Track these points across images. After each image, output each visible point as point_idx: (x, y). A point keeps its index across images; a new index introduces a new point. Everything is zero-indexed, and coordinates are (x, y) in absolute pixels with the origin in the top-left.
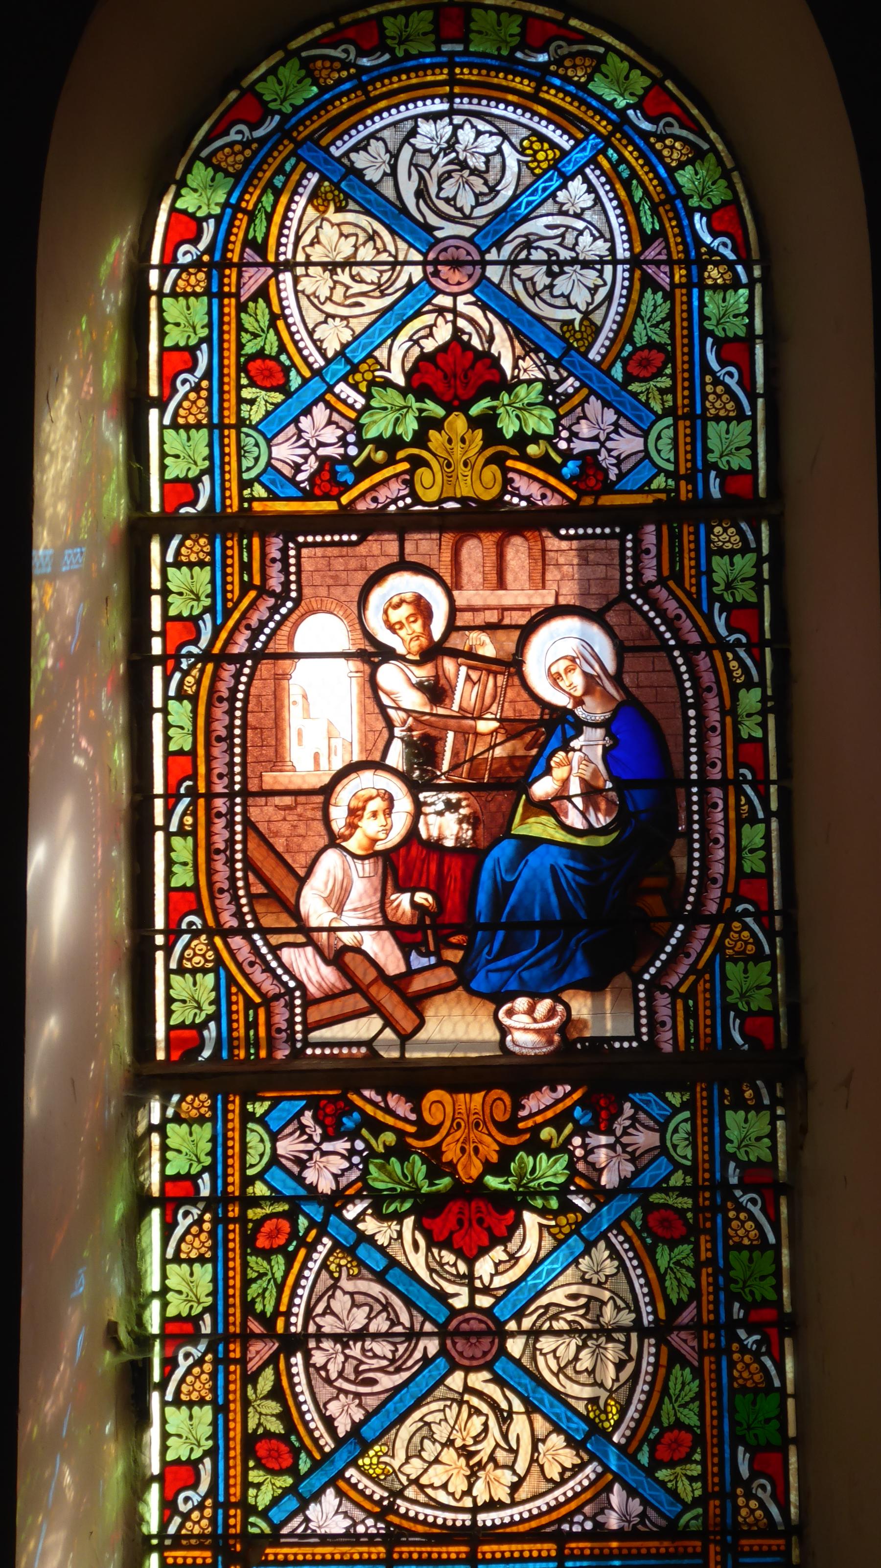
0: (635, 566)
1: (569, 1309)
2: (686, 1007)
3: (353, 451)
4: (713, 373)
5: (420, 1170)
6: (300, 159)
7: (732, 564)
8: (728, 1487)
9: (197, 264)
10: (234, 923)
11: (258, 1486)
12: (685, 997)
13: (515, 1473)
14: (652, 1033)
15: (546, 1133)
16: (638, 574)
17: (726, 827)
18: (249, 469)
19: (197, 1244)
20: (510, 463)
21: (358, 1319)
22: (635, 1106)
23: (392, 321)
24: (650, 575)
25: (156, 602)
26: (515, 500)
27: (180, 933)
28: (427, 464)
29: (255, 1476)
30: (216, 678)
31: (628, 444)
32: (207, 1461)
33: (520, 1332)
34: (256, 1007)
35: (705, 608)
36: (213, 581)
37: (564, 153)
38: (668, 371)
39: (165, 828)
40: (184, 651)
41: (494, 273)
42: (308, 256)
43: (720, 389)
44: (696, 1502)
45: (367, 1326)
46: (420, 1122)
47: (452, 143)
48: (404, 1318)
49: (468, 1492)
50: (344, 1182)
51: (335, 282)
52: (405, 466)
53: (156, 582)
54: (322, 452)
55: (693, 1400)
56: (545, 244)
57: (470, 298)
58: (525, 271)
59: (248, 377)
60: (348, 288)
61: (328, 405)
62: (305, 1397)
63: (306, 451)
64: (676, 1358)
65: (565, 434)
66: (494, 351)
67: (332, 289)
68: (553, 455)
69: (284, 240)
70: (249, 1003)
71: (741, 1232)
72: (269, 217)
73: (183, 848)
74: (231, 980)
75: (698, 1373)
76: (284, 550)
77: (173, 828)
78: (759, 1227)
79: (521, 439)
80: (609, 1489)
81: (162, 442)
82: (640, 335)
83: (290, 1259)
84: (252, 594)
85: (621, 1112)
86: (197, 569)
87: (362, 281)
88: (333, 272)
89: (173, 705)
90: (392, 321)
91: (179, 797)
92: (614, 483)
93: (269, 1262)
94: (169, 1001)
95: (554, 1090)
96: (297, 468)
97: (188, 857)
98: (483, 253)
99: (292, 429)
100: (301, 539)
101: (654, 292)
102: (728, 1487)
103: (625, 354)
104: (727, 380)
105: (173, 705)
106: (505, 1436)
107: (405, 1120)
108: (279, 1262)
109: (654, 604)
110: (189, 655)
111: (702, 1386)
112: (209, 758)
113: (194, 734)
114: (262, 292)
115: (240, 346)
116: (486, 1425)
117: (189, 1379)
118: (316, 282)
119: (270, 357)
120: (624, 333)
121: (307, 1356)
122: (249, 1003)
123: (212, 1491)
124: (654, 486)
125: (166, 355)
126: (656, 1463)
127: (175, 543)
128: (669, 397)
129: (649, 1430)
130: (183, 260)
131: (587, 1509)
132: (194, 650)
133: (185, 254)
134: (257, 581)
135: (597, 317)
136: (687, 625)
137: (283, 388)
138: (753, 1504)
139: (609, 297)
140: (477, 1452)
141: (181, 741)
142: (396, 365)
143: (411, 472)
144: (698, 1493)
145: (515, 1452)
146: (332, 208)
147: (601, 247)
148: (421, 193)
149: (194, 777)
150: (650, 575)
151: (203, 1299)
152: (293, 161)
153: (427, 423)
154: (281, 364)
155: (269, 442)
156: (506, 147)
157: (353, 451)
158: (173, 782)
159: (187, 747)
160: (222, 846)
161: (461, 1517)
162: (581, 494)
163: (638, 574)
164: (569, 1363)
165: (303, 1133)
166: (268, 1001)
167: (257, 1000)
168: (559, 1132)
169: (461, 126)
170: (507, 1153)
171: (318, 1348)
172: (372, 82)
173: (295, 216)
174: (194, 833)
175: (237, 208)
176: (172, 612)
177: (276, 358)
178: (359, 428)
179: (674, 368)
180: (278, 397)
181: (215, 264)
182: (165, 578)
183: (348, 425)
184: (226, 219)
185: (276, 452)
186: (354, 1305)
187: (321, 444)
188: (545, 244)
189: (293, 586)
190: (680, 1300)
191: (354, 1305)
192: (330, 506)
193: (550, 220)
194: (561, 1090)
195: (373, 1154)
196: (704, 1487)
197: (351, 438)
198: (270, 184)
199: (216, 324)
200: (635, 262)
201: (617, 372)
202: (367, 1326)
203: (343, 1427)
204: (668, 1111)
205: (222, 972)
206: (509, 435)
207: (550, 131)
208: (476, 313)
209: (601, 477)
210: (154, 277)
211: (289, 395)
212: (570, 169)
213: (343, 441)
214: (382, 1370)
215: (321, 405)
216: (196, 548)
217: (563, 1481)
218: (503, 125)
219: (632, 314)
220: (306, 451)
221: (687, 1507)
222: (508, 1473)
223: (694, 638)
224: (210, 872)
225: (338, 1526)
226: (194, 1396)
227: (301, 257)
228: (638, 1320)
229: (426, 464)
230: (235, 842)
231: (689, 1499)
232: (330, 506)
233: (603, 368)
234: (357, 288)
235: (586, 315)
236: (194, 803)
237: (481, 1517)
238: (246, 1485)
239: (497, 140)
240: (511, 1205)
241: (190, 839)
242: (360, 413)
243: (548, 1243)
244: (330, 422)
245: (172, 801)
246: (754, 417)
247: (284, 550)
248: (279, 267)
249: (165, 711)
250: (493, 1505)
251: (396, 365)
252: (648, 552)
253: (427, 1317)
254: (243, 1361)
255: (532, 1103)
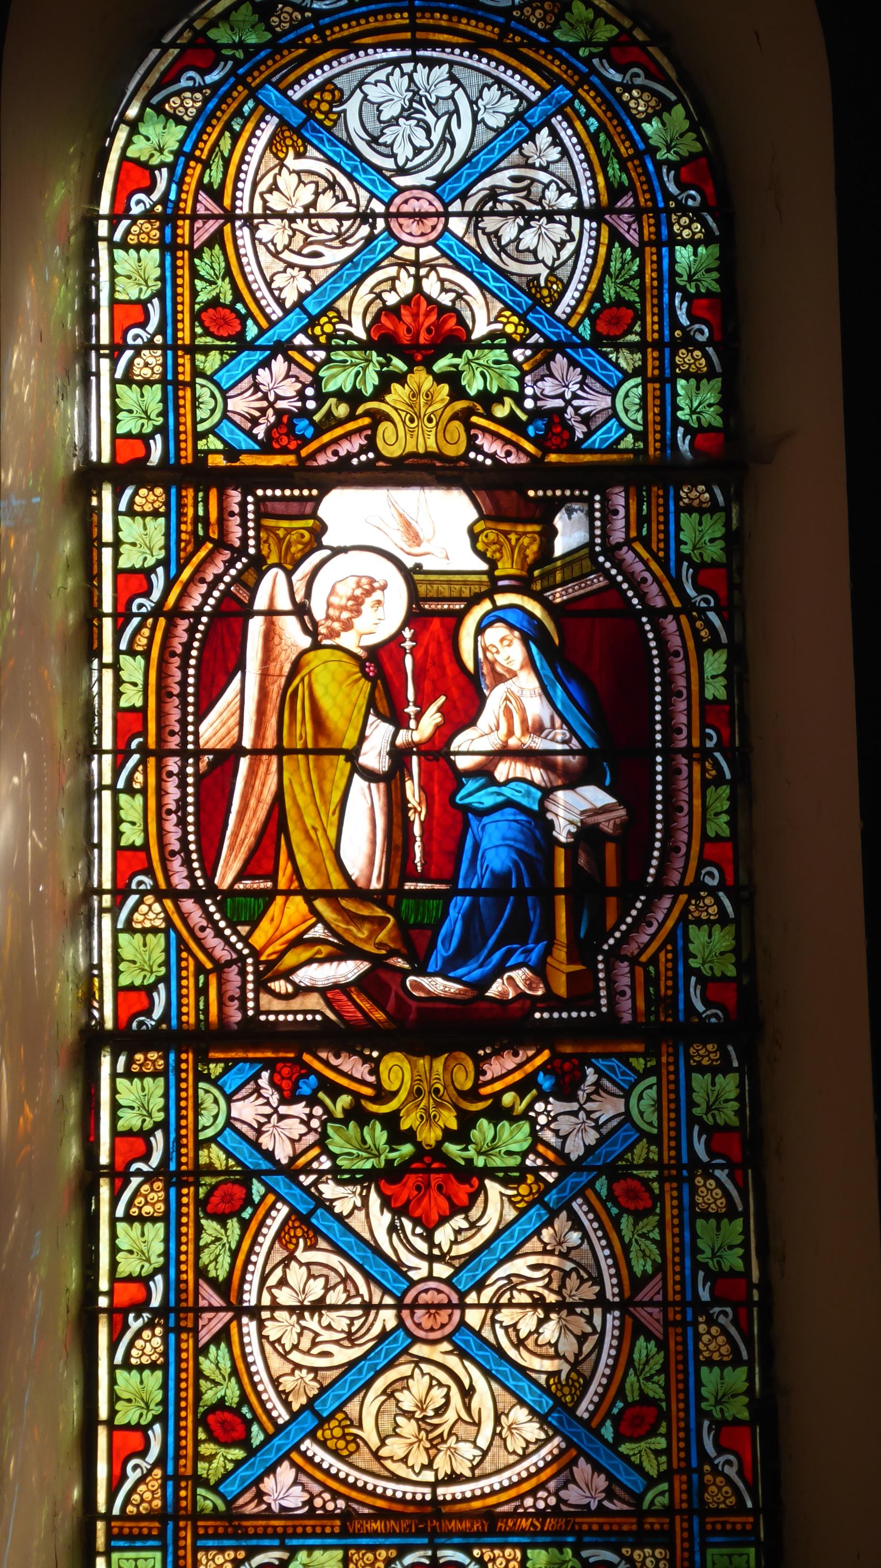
0: (603, 528)
1: (322, 243)
2: (647, 973)
3: (311, 405)
4: (710, 1461)
5: (379, 1135)
6: (258, 102)
7: (713, 1084)
8: (694, 1464)
9: (148, 215)
10: (185, 885)
11: (210, 1459)
12: (645, 966)
13: (476, 1447)
14: (612, 1003)
15: (508, 1099)
16: (605, 536)
17: (691, 795)
18: (650, 1087)
19: (148, 1350)
20: (474, 419)
21: (316, 1289)
22: (598, 1071)
23: (352, 274)
24: (618, 536)
25: (107, 554)
26: (480, 458)
27: (129, 892)
28: (388, 418)
29: (207, 1449)
30: (168, 635)
31: (247, 1110)
32: (157, 1427)
33: (478, 1306)
34: (207, 973)
35: (673, 572)
36: (164, 1387)
37: (312, 1435)
38: (663, 1430)
39: (113, 787)
40: (133, 1168)
41: (474, 1318)
42: (274, 1298)
43: (714, 1330)
44: (663, 1476)
45: (323, 1298)
46: (378, 1086)
47: (435, 1445)
48: (363, 1290)
49: (429, 1466)
50: (300, 1147)
51: (303, 1328)
52: (484, 1091)
53: (107, 536)
54: (280, 404)
55: (658, 1373)
56: (530, 1287)
57: (415, 1275)
58: (490, 223)
59: (202, 325)
60: (546, 1287)
61: (293, 1464)
62: (259, 1366)
63: (265, 404)
64: (640, 1330)
65: (315, 1123)
66: (387, 1217)
67: (300, 1335)
68: (519, 412)
69: (239, 194)
70: (200, 969)
71: (712, 1347)
72: (227, 162)
73: (131, 807)
74: (180, 939)
75: (662, 1345)
76: (243, 504)
77: (121, 785)
78: (731, 1340)
79: (487, 399)
80: (574, 1462)
81: (114, 1091)
82: (610, 291)
83: (245, 1225)
84: (644, 959)
85: (585, 1076)
86: (147, 1373)
87: (321, 231)
88: (301, 1317)
89: (124, 660)
90: (352, 274)
91: (129, 754)
92: (264, 1069)
93: (224, 1226)
94: (115, 1106)
95: (516, 1054)
96: (255, 422)
97: (137, 817)
98: (446, 205)
99: (248, 381)
100: (260, 492)
101: (648, 1340)
102: (694, 1464)
103: (615, 1411)
104: (727, 1470)
105: (124, 660)
106: (468, 1409)
107: (362, 1082)
108: (233, 1225)
109: (618, 564)
110: (139, 1173)
111: (667, 1358)
112: (161, 715)
113: (146, 830)
114: (217, 239)
115: (194, 293)
116: (447, 1397)
117: (139, 1343)
118: (281, 1328)
119: (230, 1409)
120: (615, 1387)
121: (261, 1326)
122: (200, 969)
123: (160, 1462)
124: (622, 446)
125: (117, 307)
126: (620, 1438)
127: (128, 492)
128: (664, 1459)
129: (613, 1405)
130: (136, 210)
131: (552, 1485)
132: (144, 1167)
133: (138, 204)
134: (639, 971)
135: (271, 161)
136: (654, 589)
137: (244, 1442)
138: (711, 1183)
139: (577, 252)
140: (436, 1426)
141: (132, 698)
142: (357, 319)
143: (374, 427)
144: (664, 1467)
145: (478, 1425)
146: (291, 153)
147: (589, 1292)
148: (467, 1393)
149: (144, 733)
150: (618, 536)
151: (154, 1259)
152: (251, 104)
153: (387, 379)
154: (237, 312)
155: (229, 1099)
156: (374, 1442)
157: (311, 405)
158: (123, 601)
159: (139, 842)
160: (173, 807)
161: (420, 1489)
162: (299, 1062)
163: (605, 536)
164: (530, 1334)
165: (260, 1095)
166: (220, 967)
167: (209, 965)
168: (329, 412)
169: (423, 1467)
170: (467, 1121)
171: (273, 1318)
172: (330, 26)
173: (254, 161)
174: (144, 791)
175: (190, 156)
176: (124, 842)
177: (231, 307)
178: (317, 382)
179: (197, 1193)
180: (238, 1454)
181: (168, 216)
182: (117, 528)
183: (308, 379)
184: (179, 170)
185: (232, 405)
186: (310, 1276)
187: (278, 398)
188: (530, 1287)
189: (252, 542)
190: (644, 1272)
191: (310, 1276)
192: (289, 460)
193: (533, 1260)
194: (522, 1057)
195: (331, 1118)
196: (669, 1462)
197: (310, 392)
198: (228, 127)
199: (168, 279)
200: (625, 1305)
201: (608, 1432)
202: (323, 1298)
203: (290, 297)
204: (632, 1078)
205: (173, 935)
206: (472, 392)
207: (328, 1460)
208: (408, 1259)
209: (566, 435)
210: (103, 228)
211: (252, 1452)
212: (535, 121)
213: (301, 396)
214: (337, 1342)
215: (286, 1464)
216: (148, 498)
217: (524, 1457)
218: (375, 1467)
219: (624, 1361)
220: (265, 404)
221: (652, 1482)
222: (470, 1446)
223: (659, 602)
224: (161, 833)
225: (295, 1499)
226: (145, 1360)
227: (266, 1300)
228: (602, 1293)
229: (388, 418)
230: (186, 804)
231: (654, 1473)
232: (289, 460)
233: (591, 1427)
234: (326, 1335)
235: (552, 269)
236: (143, 762)
237: (440, 1491)
238: (197, 1457)
239: (383, 1452)
240: (473, 1178)
241: (139, 798)
242: (319, 366)
243: (510, 1214)
244: (296, 1483)
245: (121, 620)
246: (745, 1215)
247: (243, 504)
248: (239, 1311)
249: (116, 667)
250: (453, 1478)
251: (357, 319)
252: (623, 993)
253: (386, 1291)
254: (195, 1331)
255: (494, 1068)
